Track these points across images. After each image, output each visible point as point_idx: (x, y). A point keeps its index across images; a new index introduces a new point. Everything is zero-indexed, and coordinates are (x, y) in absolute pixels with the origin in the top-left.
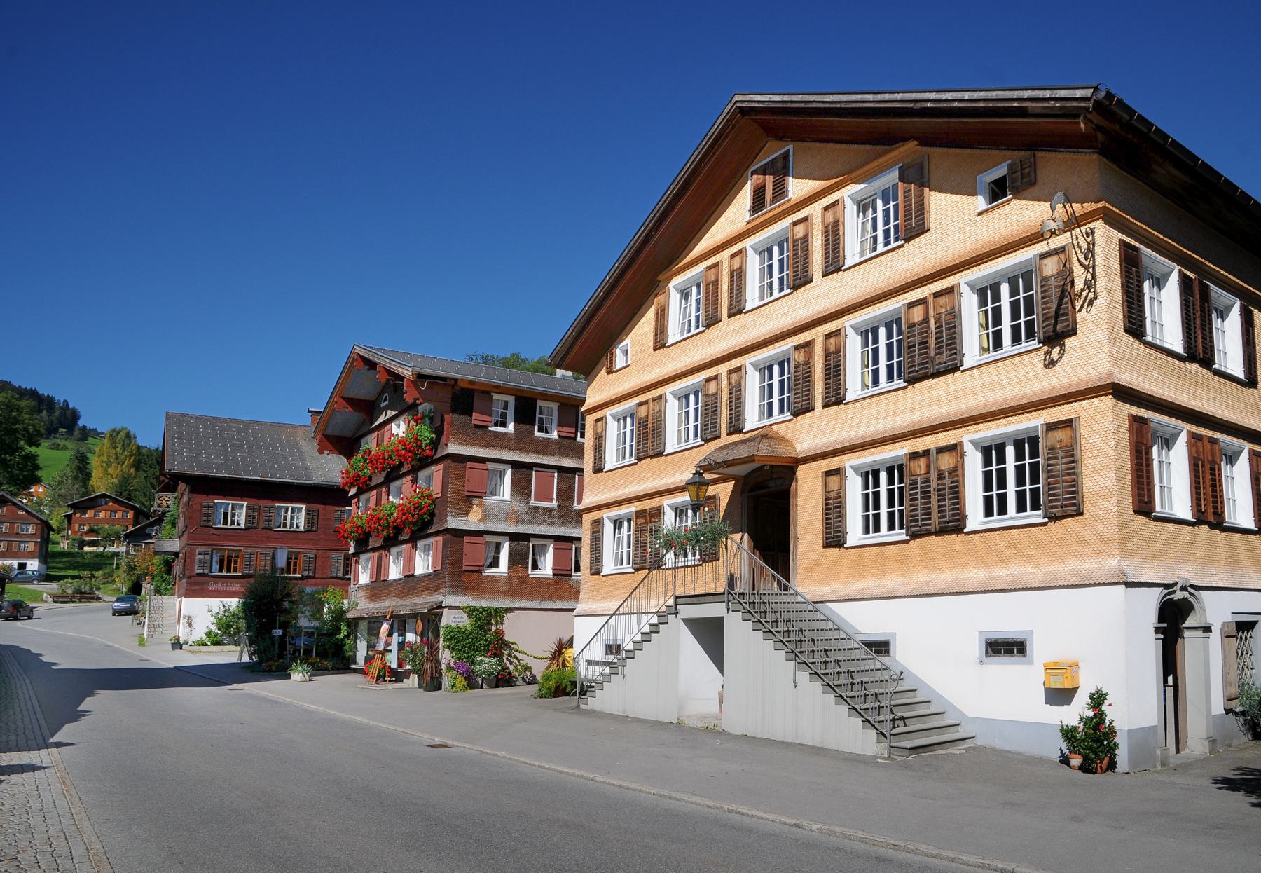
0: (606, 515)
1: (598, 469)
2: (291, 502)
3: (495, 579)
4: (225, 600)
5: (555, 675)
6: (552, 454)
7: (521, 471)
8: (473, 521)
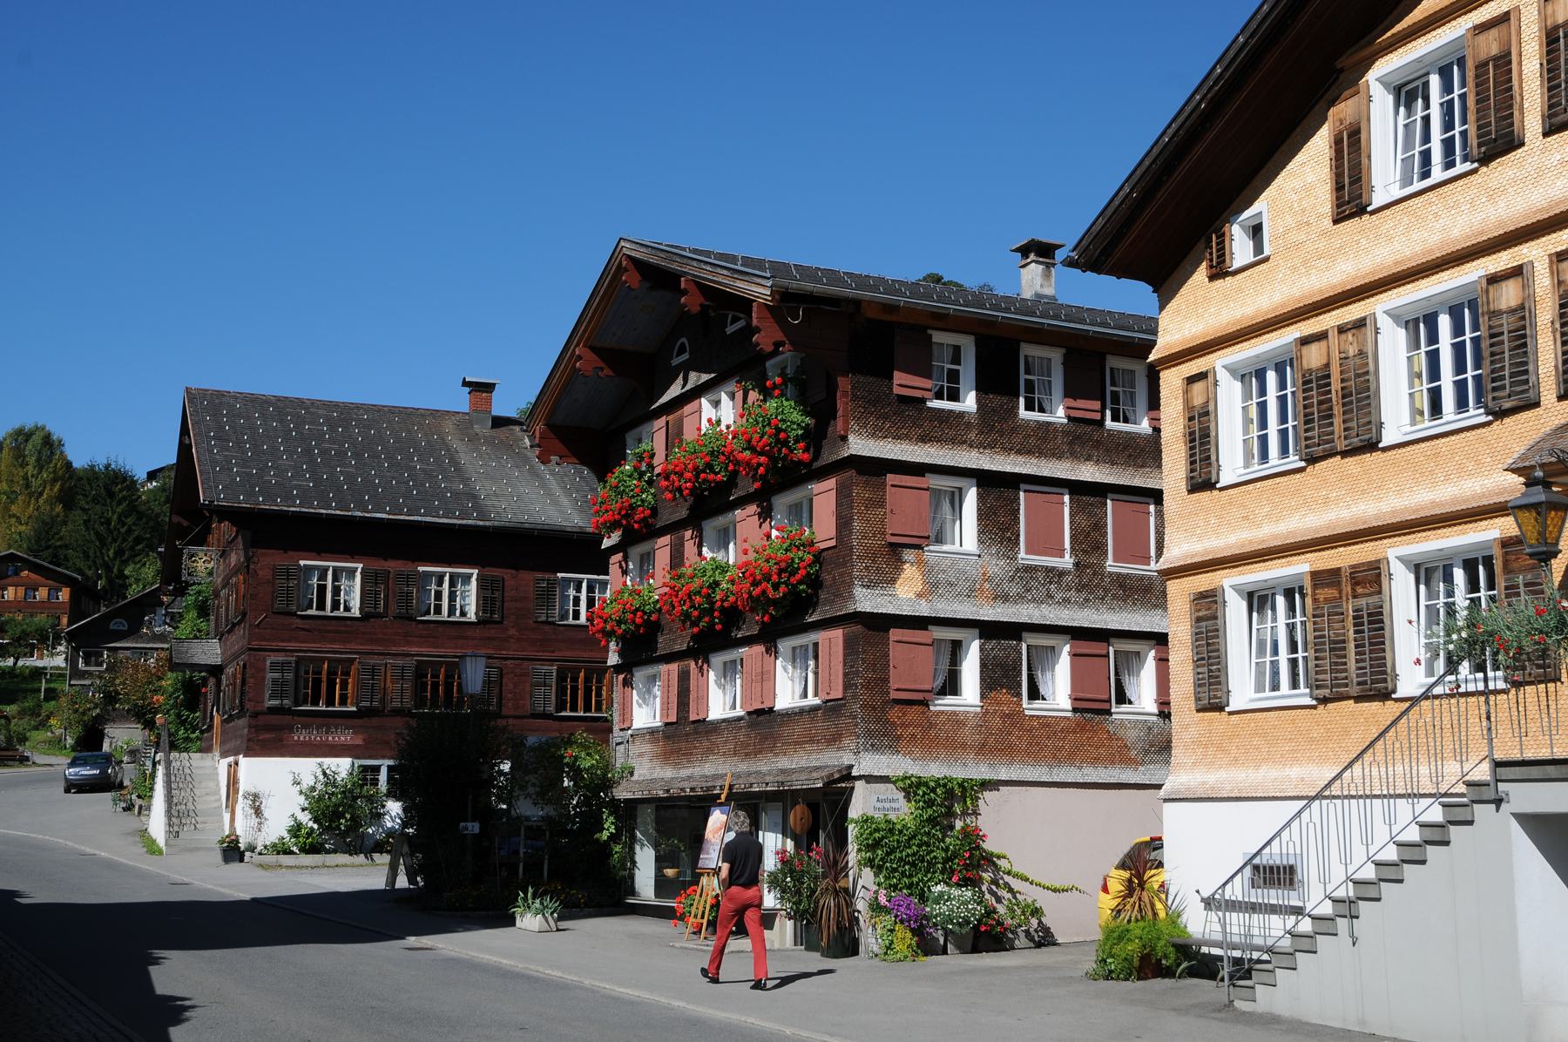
0: (1230, 582)
1: (1202, 481)
2: (450, 565)
3: (956, 720)
4: (327, 761)
5: (1137, 929)
6: (1057, 455)
7: (995, 492)
8: (905, 594)
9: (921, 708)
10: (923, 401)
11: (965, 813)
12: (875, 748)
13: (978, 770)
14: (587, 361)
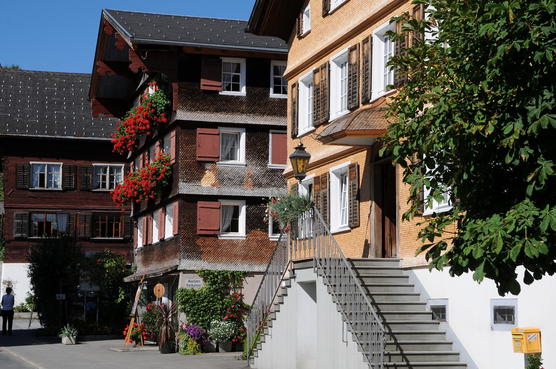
2: (110, 162)
3: (232, 244)
8: (207, 184)
9: (213, 238)
10: (217, 92)
11: (235, 287)
12: (189, 257)
13: (245, 268)
14: (103, 68)
